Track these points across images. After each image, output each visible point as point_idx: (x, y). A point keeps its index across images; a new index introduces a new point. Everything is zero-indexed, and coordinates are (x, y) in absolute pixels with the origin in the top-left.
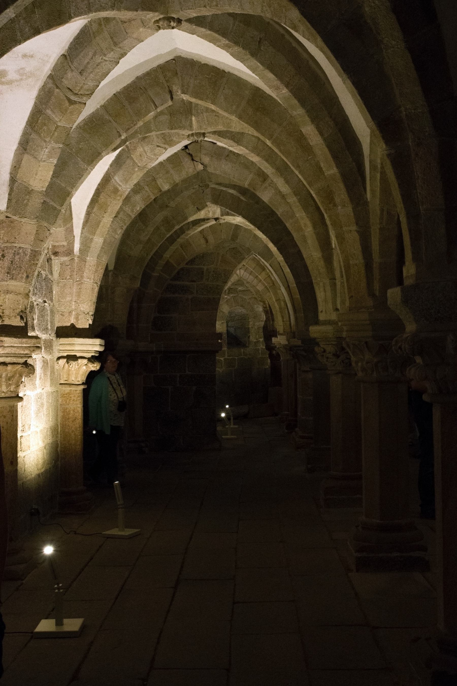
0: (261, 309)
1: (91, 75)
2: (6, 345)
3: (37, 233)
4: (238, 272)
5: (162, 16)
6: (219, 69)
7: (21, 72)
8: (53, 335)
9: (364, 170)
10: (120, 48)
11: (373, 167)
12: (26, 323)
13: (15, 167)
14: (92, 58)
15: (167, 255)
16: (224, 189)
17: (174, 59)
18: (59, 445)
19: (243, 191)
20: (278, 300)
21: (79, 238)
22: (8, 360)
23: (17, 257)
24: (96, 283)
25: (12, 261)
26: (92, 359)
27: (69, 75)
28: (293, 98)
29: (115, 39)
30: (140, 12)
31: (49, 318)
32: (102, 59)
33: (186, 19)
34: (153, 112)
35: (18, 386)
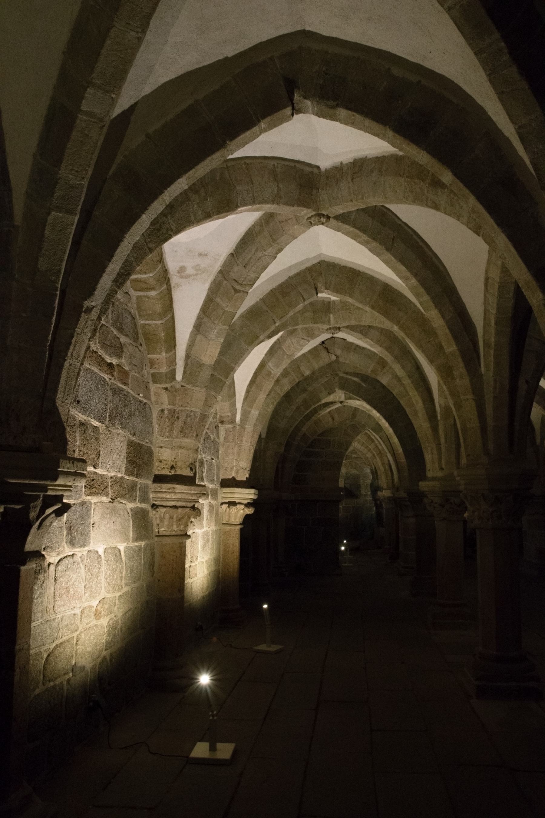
0: (368, 471)
1: (253, 267)
2: (177, 491)
3: (206, 400)
4: (353, 444)
5: (314, 213)
6: (355, 270)
7: (197, 268)
8: (218, 485)
9: (479, 348)
10: (278, 244)
11: (487, 345)
12: (195, 474)
13: (190, 345)
14: (254, 254)
15: (304, 429)
16: (350, 377)
17: (319, 263)
18: (221, 573)
19: (365, 378)
20: (383, 464)
21: (240, 411)
22: (179, 504)
23: (189, 419)
24: (253, 446)
25: (185, 422)
26: (248, 505)
27: (236, 269)
28: (421, 286)
29: (274, 237)
30: (296, 208)
31: (215, 472)
32: (262, 254)
33: (334, 216)
34: (301, 304)
35: (186, 526)
